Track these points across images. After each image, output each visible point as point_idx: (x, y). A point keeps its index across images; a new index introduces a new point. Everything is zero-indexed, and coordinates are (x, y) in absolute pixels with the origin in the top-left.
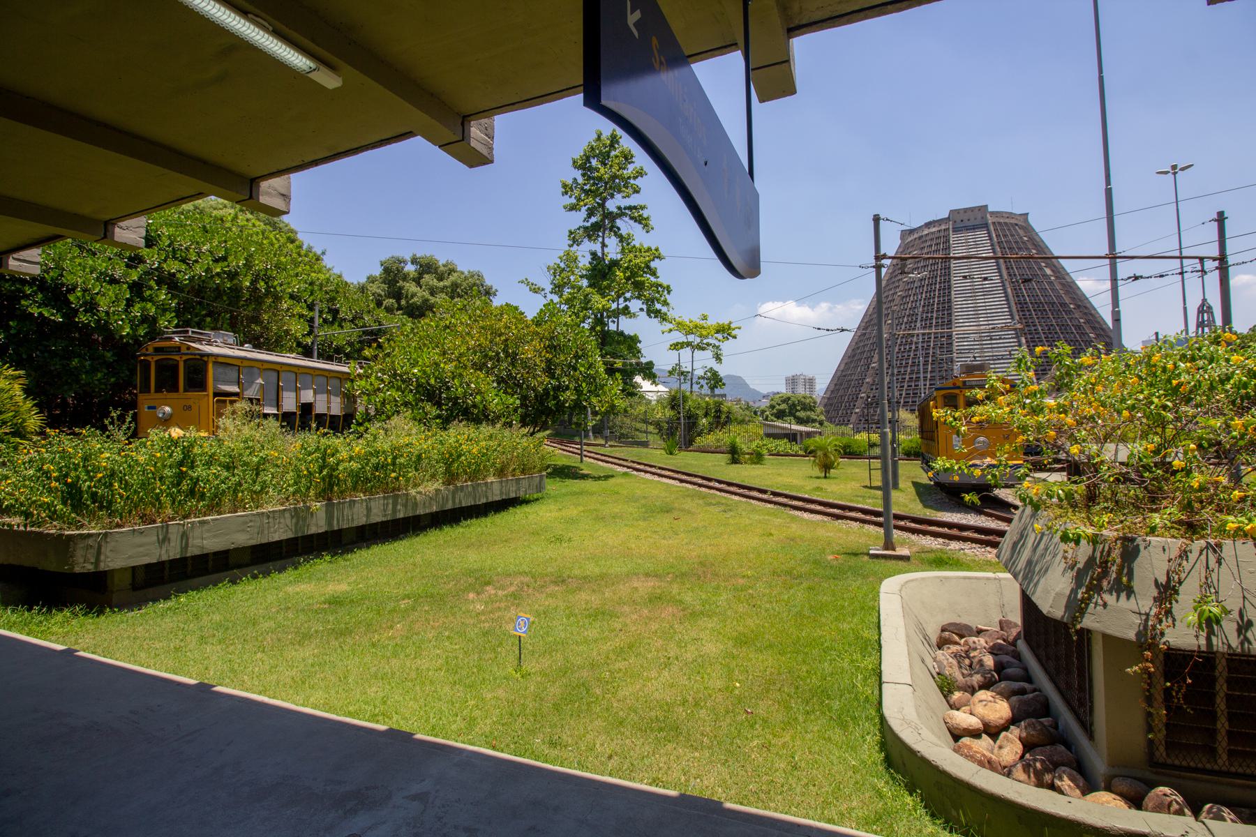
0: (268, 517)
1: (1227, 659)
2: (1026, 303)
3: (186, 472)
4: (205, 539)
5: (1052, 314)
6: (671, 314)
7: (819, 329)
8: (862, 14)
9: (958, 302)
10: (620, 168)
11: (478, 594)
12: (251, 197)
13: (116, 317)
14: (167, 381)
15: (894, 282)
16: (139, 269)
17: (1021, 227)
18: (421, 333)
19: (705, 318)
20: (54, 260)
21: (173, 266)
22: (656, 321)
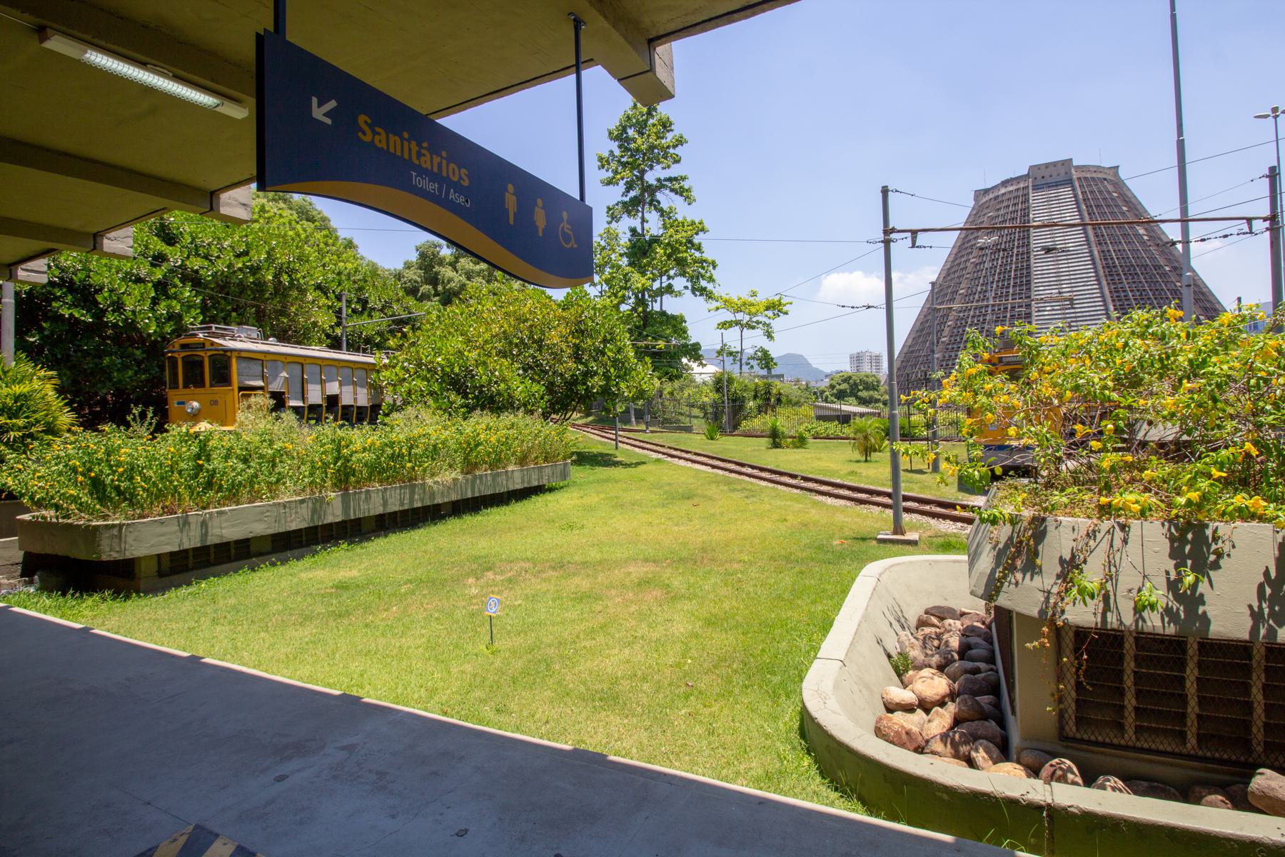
0: (285, 507)
1: (1199, 643)
2: (1115, 267)
3: (203, 465)
4: (224, 528)
5: (1145, 278)
6: (717, 291)
7: (843, 306)
8: (713, 22)
10: (658, 138)
11: (477, 579)
12: (212, 209)
13: (142, 316)
14: (194, 377)
16: (163, 268)
18: (447, 321)
19: (754, 294)
20: (81, 262)
21: (195, 263)
22: (701, 299)
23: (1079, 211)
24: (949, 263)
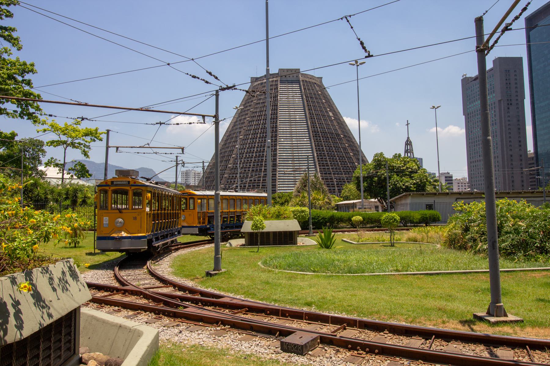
2: (318, 132)
5: (331, 140)
9: (282, 128)
15: (245, 111)
17: (318, 86)
22: (30, 122)
23: (302, 99)
24: (236, 119)
